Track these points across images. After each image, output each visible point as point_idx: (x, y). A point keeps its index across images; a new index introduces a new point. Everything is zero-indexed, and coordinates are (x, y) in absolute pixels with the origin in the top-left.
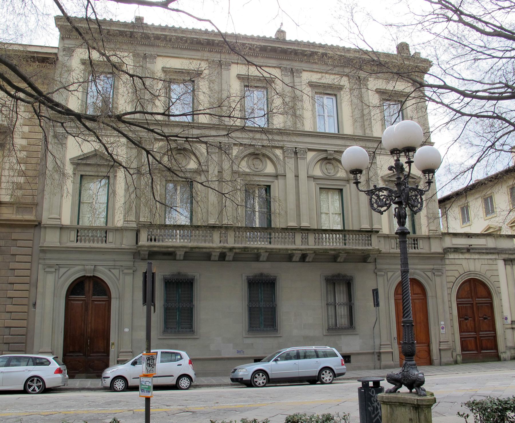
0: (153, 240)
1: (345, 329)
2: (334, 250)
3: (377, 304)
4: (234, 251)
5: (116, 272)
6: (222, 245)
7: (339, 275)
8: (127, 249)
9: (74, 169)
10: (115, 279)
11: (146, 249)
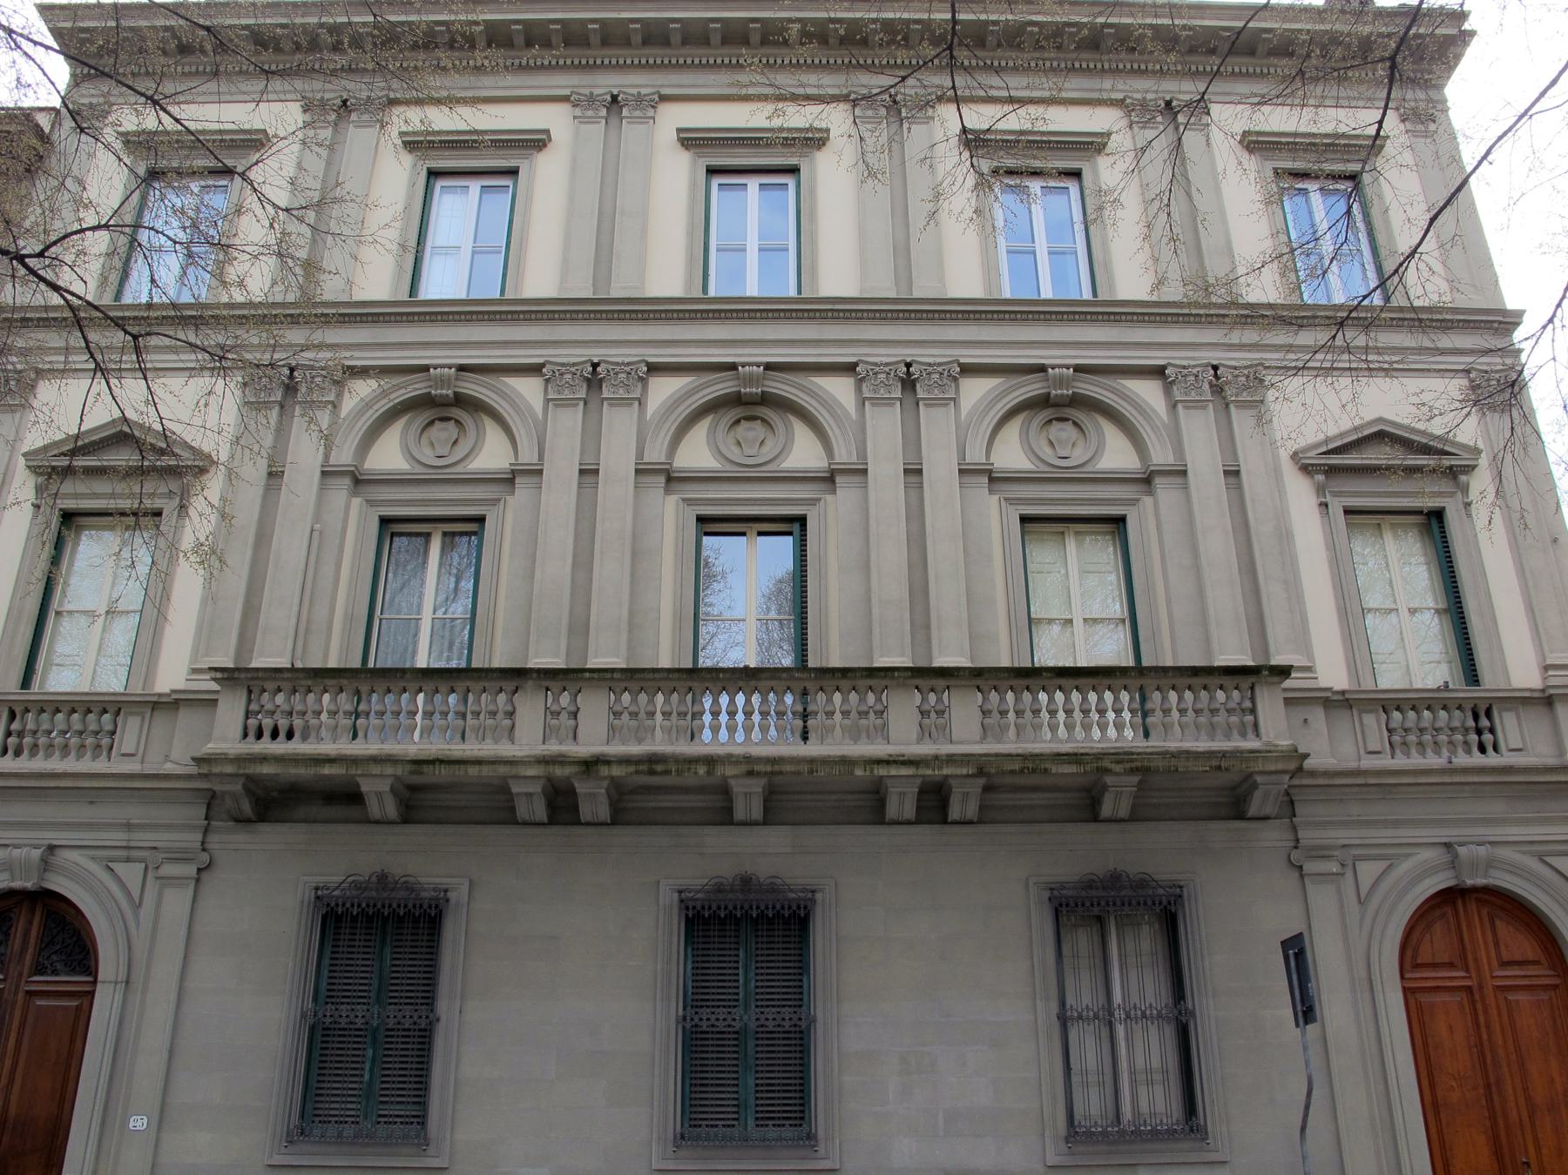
0: (267, 734)
1: (1171, 1134)
2: (1074, 758)
3: (1306, 1012)
4: (604, 771)
5: (131, 873)
6: (554, 748)
7: (1115, 878)
8: (178, 777)
9: (39, 490)
10: (124, 903)
11: (229, 769)
